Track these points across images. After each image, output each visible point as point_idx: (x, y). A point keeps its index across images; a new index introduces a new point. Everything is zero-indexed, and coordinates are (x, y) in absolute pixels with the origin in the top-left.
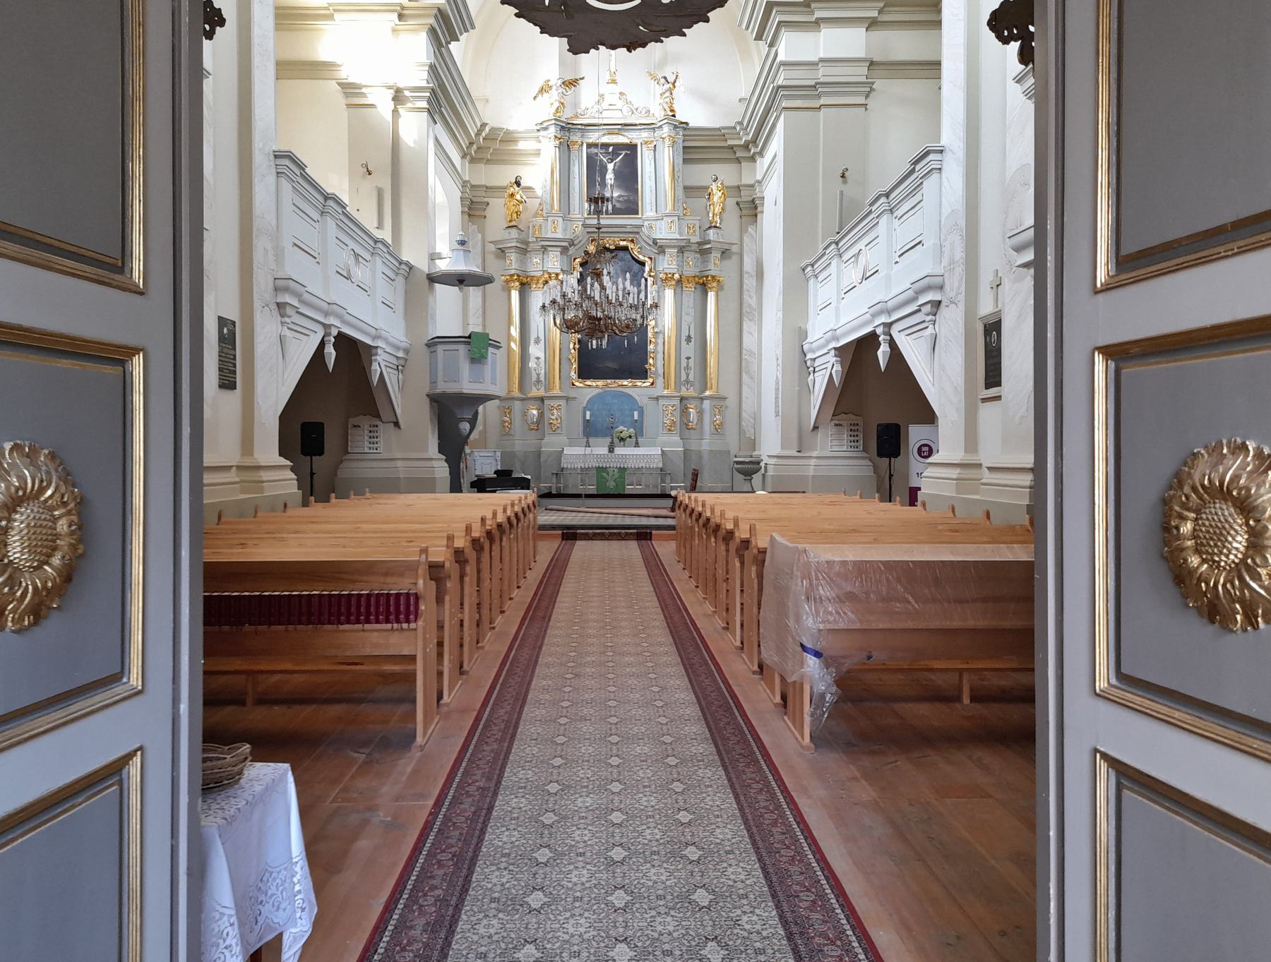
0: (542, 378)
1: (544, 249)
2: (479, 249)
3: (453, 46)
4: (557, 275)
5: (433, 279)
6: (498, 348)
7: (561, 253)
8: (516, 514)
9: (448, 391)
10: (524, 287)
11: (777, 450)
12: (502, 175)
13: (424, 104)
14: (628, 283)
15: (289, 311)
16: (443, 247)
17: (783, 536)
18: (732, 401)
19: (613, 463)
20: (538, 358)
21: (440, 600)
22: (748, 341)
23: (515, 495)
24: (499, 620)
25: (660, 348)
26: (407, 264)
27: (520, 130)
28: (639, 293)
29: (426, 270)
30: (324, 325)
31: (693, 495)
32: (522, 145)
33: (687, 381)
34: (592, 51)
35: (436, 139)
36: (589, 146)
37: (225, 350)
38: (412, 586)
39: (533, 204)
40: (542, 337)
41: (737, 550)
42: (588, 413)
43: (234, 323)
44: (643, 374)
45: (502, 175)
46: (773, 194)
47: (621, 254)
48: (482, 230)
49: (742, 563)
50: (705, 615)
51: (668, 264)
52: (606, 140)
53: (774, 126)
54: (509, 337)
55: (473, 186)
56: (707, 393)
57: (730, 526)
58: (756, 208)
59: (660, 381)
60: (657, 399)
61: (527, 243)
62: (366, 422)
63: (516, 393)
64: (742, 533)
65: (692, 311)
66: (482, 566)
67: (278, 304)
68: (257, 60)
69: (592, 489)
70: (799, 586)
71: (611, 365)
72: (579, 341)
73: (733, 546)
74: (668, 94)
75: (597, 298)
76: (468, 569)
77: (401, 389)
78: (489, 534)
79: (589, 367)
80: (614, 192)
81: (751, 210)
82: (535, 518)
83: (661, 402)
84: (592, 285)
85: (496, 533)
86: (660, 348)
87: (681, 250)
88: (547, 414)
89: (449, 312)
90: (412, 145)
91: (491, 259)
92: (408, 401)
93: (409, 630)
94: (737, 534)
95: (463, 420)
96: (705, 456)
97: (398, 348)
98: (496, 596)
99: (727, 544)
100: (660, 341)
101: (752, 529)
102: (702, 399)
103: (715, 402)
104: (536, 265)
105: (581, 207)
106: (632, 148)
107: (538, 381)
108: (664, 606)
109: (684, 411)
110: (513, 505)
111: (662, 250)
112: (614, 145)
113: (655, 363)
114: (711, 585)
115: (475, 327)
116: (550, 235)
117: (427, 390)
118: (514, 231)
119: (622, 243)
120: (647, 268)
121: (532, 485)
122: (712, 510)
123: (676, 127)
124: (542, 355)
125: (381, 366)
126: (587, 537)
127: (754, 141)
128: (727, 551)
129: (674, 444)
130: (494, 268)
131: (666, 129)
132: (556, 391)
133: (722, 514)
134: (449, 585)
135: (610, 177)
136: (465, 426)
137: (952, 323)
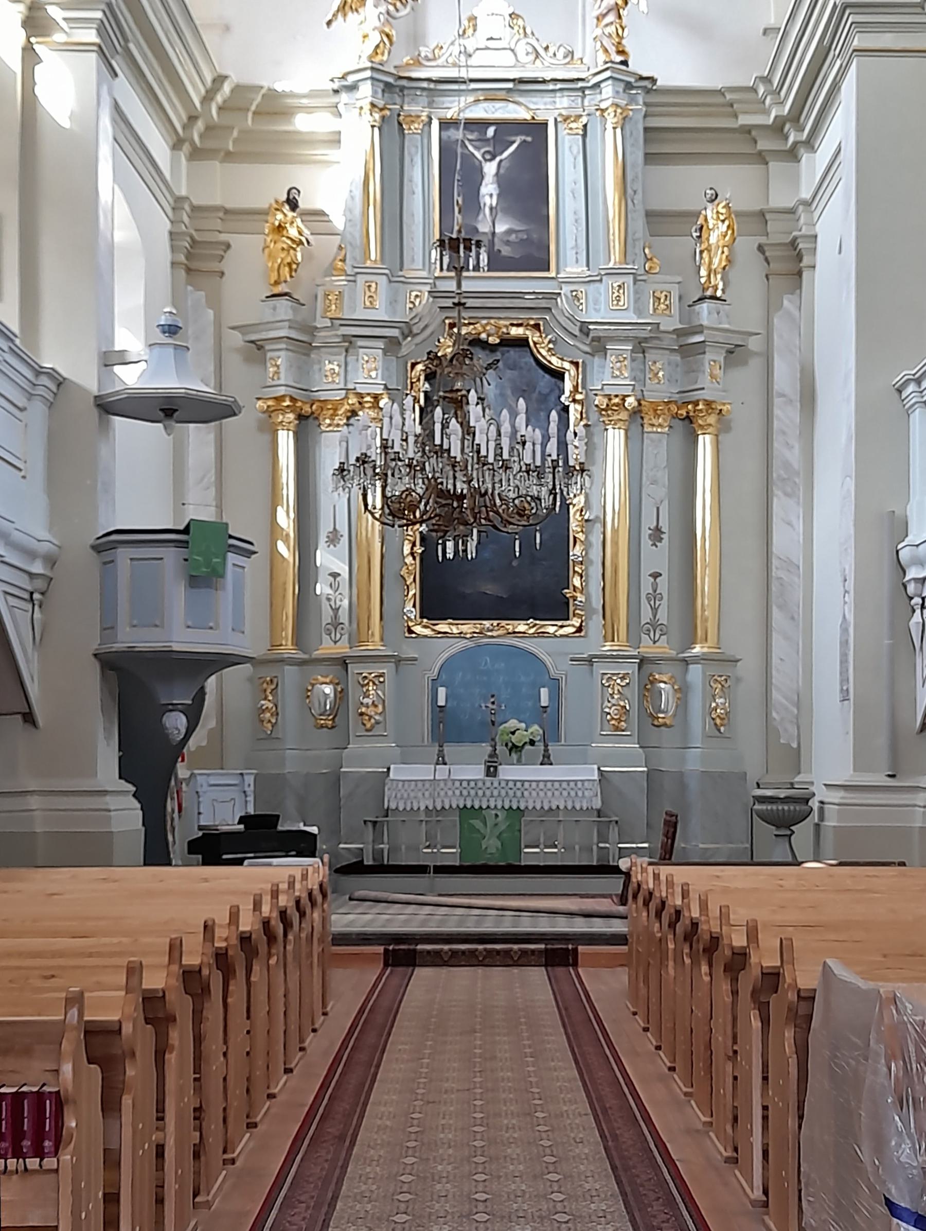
0: (344, 617)
1: (349, 343)
2: (210, 341)
4: (376, 398)
5: (108, 407)
7: (385, 352)
8: (283, 914)
9: (142, 646)
10: (306, 423)
11: (845, 774)
12: (260, 186)
13: (91, 36)
14: (521, 419)
16: (129, 338)
17: (847, 964)
18: (748, 668)
19: (494, 800)
20: (335, 575)
21: (110, 1104)
22: (784, 540)
23: (284, 870)
24: (244, 1143)
25: (595, 554)
26: (52, 374)
27: (298, 90)
28: (546, 438)
29: (94, 388)
31: (665, 871)
32: (302, 123)
33: (654, 625)
35: (116, 107)
36: (445, 124)
38: (49, 1077)
39: (326, 247)
40: (343, 529)
41: (755, 993)
44: (559, 609)
45: (260, 186)
46: (834, 230)
47: (513, 353)
48: (215, 302)
49: (765, 1022)
50: (690, 1131)
51: (612, 375)
52: (480, 112)
53: (835, 87)
54: (274, 529)
55: (194, 208)
56: (697, 649)
57: (739, 940)
58: (799, 257)
59: (596, 624)
60: (590, 661)
61: (312, 330)
63: (288, 649)
64: (765, 957)
65: (663, 476)
66: (205, 1027)
69: (450, 854)
70: (882, 1075)
71: (490, 589)
72: (423, 538)
73: (749, 979)
74: (611, 18)
75: (456, 452)
76: (174, 1036)
77: (40, 641)
78: (221, 958)
79: (443, 594)
80: (495, 223)
81: (789, 263)
82: (324, 921)
83: (600, 668)
84: (445, 426)
85: (238, 957)
86: (595, 554)
87: (641, 346)
90: (66, 124)
91: (234, 364)
93: (41, 1171)
94: (754, 959)
95: (174, 708)
96: (693, 785)
97: (32, 555)
98: (237, 1091)
99: (734, 980)
100: (596, 539)
101: (785, 948)
103: (713, 670)
104: (330, 376)
105: (427, 256)
106: (537, 129)
107: (336, 624)
108: (600, 1113)
109: (648, 688)
110: (275, 894)
111: (599, 346)
112: (501, 124)
113: (584, 586)
114: (699, 1065)
115: (200, 510)
116: (361, 314)
117: (94, 645)
118: (283, 302)
119: (515, 332)
120: (568, 386)
121: (321, 845)
122: (704, 906)
123: (629, 86)
124: (343, 570)
126: (437, 960)
127: (795, 117)
128: (735, 993)
129: (626, 757)
130: (240, 384)
131: (608, 90)
132: (375, 646)
133: (724, 914)
134: (130, 1072)
135: (489, 191)
136: (176, 722)
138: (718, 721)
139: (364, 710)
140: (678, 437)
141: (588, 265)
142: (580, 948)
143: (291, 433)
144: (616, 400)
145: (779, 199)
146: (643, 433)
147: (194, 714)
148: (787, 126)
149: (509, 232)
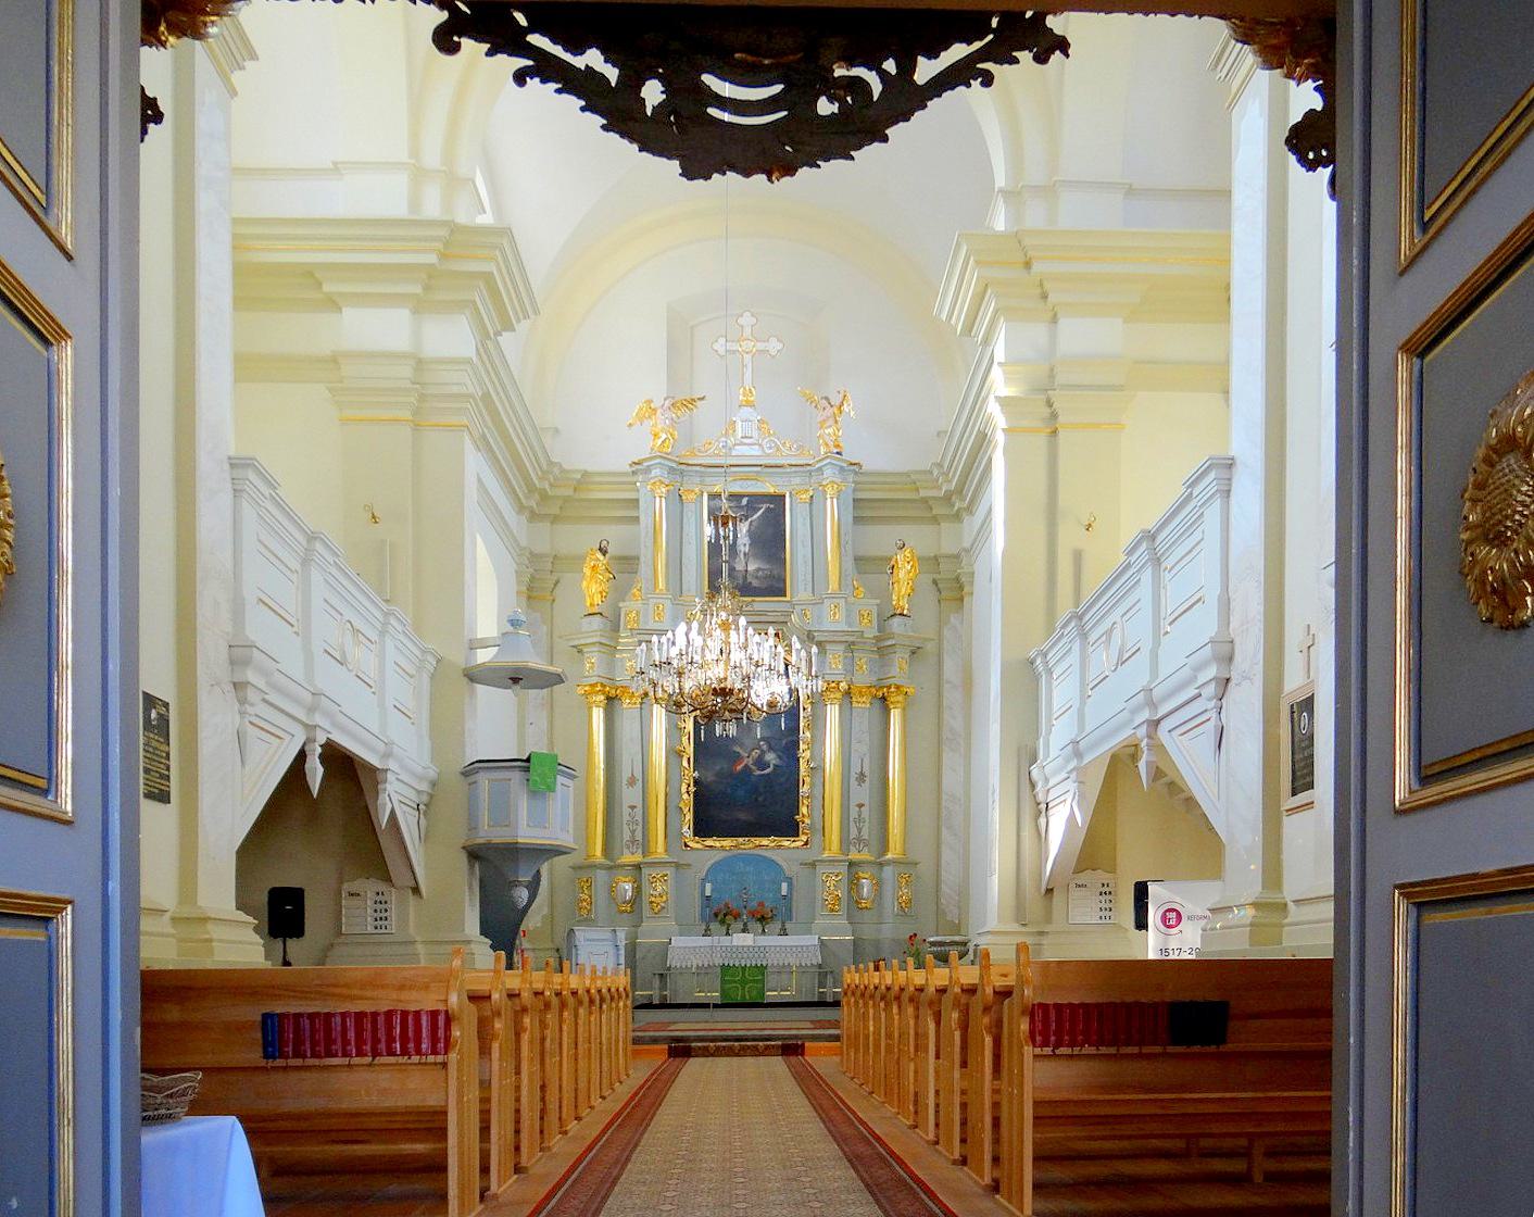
3: (506, 339)
5: (473, 676)
6: (573, 777)
15: (251, 695)
22: (951, 781)
30: (306, 726)
33: (859, 839)
34: (715, 176)
37: (154, 744)
40: (638, 775)
42: (708, 887)
43: (166, 705)
44: (792, 829)
56: (889, 856)
58: (961, 588)
60: (813, 865)
62: (369, 887)
67: (235, 684)
68: (203, 342)
87: (850, 646)
88: (647, 890)
89: (495, 725)
92: (433, 858)
97: (414, 774)
102: (881, 864)
109: (854, 883)
115: (535, 745)
117: (462, 842)
125: (396, 798)
126: (706, 1053)
127: (960, 490)
137: (1245, 710)
138: (903, 904)
139: (653, 899)
140: (877, 711)
141: (813, 593)
142: (807, 1044)
143: (601, 709)
144: (833, 685)
145: (947, 547)
146: (851, 708)
147: (534, 887)
148: (953, 498)
149: (758, 570)
